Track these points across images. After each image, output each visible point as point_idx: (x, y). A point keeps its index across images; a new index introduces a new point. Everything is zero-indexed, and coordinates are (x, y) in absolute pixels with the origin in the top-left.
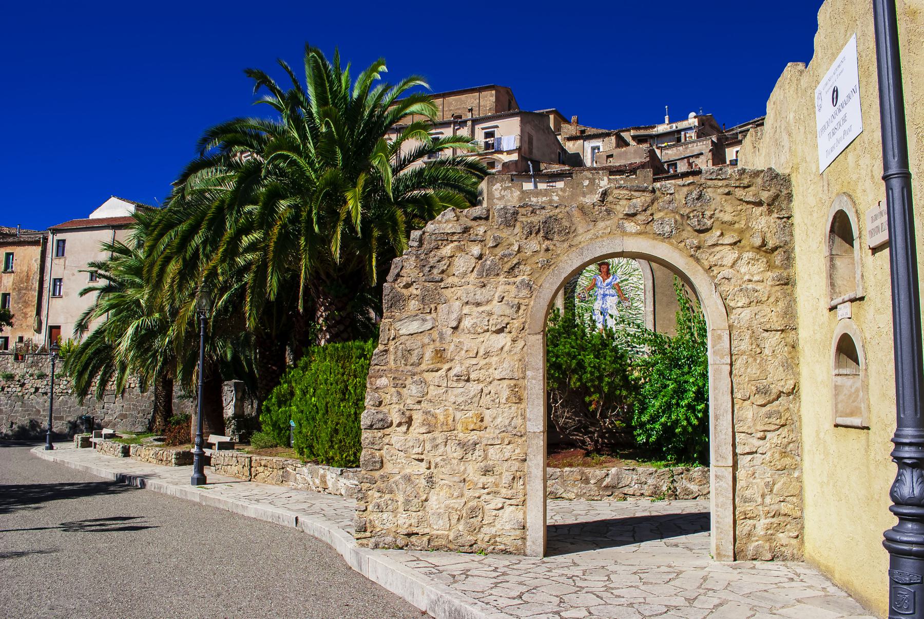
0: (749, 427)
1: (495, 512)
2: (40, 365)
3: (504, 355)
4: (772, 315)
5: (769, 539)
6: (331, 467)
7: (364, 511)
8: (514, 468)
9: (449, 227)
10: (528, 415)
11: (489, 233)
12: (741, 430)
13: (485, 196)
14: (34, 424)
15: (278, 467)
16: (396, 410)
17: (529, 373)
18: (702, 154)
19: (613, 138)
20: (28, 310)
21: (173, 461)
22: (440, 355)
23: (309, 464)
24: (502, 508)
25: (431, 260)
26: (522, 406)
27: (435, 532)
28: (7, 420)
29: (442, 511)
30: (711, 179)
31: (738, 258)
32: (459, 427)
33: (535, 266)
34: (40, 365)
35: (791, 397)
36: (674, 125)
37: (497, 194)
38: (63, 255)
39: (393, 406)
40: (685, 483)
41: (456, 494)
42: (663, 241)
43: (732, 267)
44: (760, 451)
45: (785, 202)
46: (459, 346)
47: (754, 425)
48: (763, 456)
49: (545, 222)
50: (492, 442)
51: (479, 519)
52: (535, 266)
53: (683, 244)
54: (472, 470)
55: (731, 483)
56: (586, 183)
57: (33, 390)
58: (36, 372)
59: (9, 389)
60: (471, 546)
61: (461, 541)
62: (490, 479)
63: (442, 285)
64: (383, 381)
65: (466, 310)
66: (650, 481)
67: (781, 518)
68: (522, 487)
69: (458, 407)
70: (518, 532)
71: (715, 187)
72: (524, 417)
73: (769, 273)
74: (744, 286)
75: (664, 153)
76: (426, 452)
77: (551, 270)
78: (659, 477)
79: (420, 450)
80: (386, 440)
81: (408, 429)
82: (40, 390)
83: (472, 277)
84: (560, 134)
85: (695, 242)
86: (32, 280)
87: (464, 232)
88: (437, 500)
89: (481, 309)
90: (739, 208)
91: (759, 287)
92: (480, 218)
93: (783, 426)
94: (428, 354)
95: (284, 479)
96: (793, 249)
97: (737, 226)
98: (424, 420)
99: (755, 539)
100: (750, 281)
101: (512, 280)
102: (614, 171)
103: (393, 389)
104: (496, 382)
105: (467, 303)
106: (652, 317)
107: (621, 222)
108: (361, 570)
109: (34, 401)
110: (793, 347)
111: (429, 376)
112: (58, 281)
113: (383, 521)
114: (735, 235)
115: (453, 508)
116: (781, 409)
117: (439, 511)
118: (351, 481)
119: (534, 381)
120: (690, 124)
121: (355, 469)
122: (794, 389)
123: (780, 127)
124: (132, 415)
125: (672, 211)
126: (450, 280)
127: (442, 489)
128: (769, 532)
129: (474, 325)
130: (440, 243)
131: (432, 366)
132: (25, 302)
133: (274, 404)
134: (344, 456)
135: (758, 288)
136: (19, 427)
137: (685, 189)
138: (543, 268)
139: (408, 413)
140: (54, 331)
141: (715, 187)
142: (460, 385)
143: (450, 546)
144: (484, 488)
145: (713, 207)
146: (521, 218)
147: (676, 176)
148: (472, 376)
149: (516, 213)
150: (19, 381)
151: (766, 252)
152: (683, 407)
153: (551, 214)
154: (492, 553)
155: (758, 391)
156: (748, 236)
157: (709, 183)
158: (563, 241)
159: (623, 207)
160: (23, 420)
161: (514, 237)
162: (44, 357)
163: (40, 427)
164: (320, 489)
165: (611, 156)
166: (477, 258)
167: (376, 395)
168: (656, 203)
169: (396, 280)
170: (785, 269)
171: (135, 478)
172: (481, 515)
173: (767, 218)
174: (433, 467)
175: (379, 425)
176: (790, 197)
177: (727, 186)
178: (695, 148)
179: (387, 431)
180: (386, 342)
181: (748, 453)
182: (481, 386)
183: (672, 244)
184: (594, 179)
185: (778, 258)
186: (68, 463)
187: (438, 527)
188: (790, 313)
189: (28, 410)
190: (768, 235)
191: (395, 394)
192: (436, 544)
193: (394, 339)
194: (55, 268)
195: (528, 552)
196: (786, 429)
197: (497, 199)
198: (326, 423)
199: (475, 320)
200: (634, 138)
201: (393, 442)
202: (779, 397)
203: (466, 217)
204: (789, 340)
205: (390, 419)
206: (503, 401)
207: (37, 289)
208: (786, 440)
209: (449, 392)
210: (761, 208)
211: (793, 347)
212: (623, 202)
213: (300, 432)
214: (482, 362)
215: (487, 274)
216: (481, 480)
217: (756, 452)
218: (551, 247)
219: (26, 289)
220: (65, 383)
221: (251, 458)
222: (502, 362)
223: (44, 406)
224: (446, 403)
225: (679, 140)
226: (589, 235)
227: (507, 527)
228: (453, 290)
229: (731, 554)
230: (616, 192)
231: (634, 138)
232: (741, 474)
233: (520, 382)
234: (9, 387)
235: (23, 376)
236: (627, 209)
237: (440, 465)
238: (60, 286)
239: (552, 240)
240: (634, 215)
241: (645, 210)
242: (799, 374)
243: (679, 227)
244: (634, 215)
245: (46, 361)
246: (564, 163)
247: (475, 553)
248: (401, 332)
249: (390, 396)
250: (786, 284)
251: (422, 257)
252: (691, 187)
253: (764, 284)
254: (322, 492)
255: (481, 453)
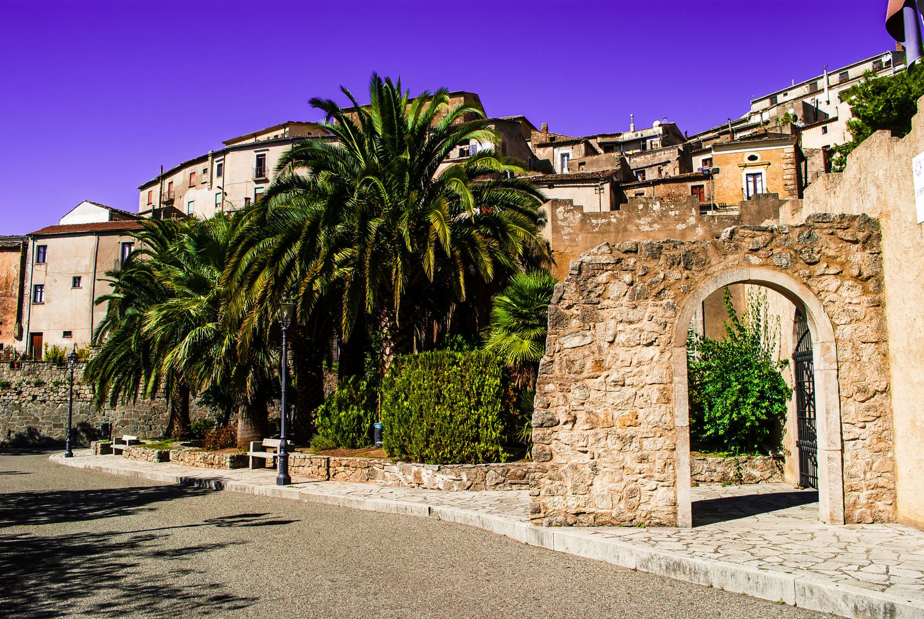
0: (853, 419)
1: (650, 493)
2: (38, 373)
3: (654, 364)
4: (867, 330)
5: (870, 506)
6: (426, 465)
7: (537, 496)
8: (665, 456)
9: (604, 259)
10: (676, 413)
11: (638, 263)
12: (846, 421)
13: (549, 218)
14: (32, 432)
15: (363, 466)
16: (563, 410)
17: (676, 379)
18: (669, 162)
19: (582, 146)
20: (8, 316)
21: (228, 464)
22: (599, 364)
23: (399, 463)
24: (656, 489)
25: (588, 285)
26: (670, 405)
27: (600, 511)
28: (5, 429)
29: (605, 493)
30: (818, 222)
31: (841, 285)
32: (618, 424)
33: (677, 291)
34: (38, 373)
35: (884, 394)
36: (639, 133)
37: (560, 216)
38: (44, 261)
39: (560, 407)
40: (749, 470)
41: (617, 479)
42: (781, 271)
43: (836, 292)
44: (861, 437)
45: (876, 241)
46: (615, 357)
47: (857, 417)
48: (864, 442)
49: (685, 255)
50: (647, 436)
51: (637, 498)
52: (677, 291)
53: (797, 274)
54: (629, 459)
55: (840, 463)
56: (641, 207)
57: (30, 398)
58: (34, 380)
59: (6, 398)
60: (631, 521)
61: (622, 517)
62: (645, 466)
63: (599, 306)
64: (550, 387)
65: (620, 327)
66: (718, 469)
67: (879, 490)
68: (672, 471)
69: (615, 407)
70: (670, 508)
71: (821, 228)
72: (672, 414)
73: (864, 297)
74: (846, 308)
75: (632, 161)
76: (589, 445)
77: (691, 294)
78: (726, 465)
79: (584, 444)
80: (554, 436)
81: (573, 427)
82: (38, 398)
83: (625, 300)
84: (530, 141)
85: (807, 272)
86: (12, 287)
87: (617, 263)
88: (601, 484)
89: (633, 326)
90: (841, 245)
91: (857, 308)
92: (631, 251)
93: (878, 417)
94: (589, 364)
95: (371, 477)
96: (883, 278)
97: (838, 259)
98: (588, 419)
99: (860, 506)
100: (850, 303)
101: (659, 303)
102: (589, 179)
103: (560, 393)
104: (648, 386)
105: (621, 322)
106: (701, 326)
107: (746, 255)
108: (542, 543)
109: (31, 409)
110: (885, 355)
111: (590, 383)
112: (39, 288)
113: (554, 504)
114: (838, 267)
115: (615, 491)
116: (877, 404)
117: (603, 493)
118: (449, 476)
119: (680, 385)
120: (654, 132)
121: (452, 466)
122: (886, 388)
123: (865, 179)
124: (133, 421)
125: (788, 248)
126: (605, 303)
127: (605, 474)
128: (870, 501)
129: (628, 340)
130: (596, 271)
131: (593, 374)
132: (4, 308)
133: (334, 409)
134: (440, 454)
135: (857, 309)
136: (16, 435)
137: (798, 230)
138: (685, 293)
139: (573, 413)
140: (36, 338)
141: (821, 228)
142: (617, 389)
143: (614, 522)
144: (640, 473)
145: (820, 244)
146: (664, 251)
147: (647, 184)
148: (628, 382)
149: (660, 248)
150: (16, 389)
151: (861, 280)
152: (749, 404)
153: (690, 248)
154: (648, 526)
155: (859, 391)
156: (848, 267)
157: (817, 225)
158: (700, 271)
159: (748, 244)
160: (20, 428)
161: (660, 268)
162: (41, 364)
163: (38, 434)
164: (413, 485)
165: (583, 164)
166: (628, 285)
167: (545, 398)
168: (774, 241)
169: (559, 302)
170: (877, 294)
171: (209, 480)
172: (638, 495)
173: (862, 253)
174: (596, 457)
175: (549, 424)
176: (879, 237)
177: (831, 228)
178: (663, 156)
179: (555, 428)
180: (552, 354)
181: (852, 440)
182: (634, 390)
183: (788, 274)
184: (648, 204)
185: (871, 285)
186: (107, 469)
187: (603, 506)
188: (881, 329)
189: (26, 419)
190: (863, 267)
191: (562, 398)
192: (601, 520)
193: (559, 351)
194: (36, 275)
195: (679, 524)
196: (881, 420)
197: (561, 220)
198: (420, 424)
199: (628, 336)
200: (600, 145)
201: (560, 437)
202: (875, 394)
203: (618, 250)
204: (882, 350)
205: (557, 419)
206: (655, 401)
207: (17, 295)
208: (881, 428)
209: (608, 394)
210: (857, 246)
211: (885, 355)
212: (748, 240)
213: (391, 434)
214: (636, 370)
215: (637, 297)
216: (638, 467)
217: (858, 439)
218: (690, 276)
219: (5, 295)
220: (64, 390)
221: (328, 459)
222: (652, 369)
223: (43, 414)
224: (605, 404)
225: (644, 147)
226: (721, 267)
227: (661, 504)
228: (608, 310)
229: (842, 519)
230: (743, 231)
231: (600, 145)
232: (847, 456)
233: (668, 386)
234: (5, 395)
235: (20, 384)
236: (751, 245)
237: (602, 456)
238: (41, 292)
239: (690, 270)
240: (757, 250)
241: (766, 247)
242: (890, 376)
243: (794, 260)
244: (757, 250)
245: (43, 369)
246: (535, 170)
247: (635, 526)
248: (565, 346)
249: (557, 399)
250: (878, 306)
251: (581, 283)
252: (802, 228)
253: (861, 306)
254: (416, 487)
255: (638, 445)
